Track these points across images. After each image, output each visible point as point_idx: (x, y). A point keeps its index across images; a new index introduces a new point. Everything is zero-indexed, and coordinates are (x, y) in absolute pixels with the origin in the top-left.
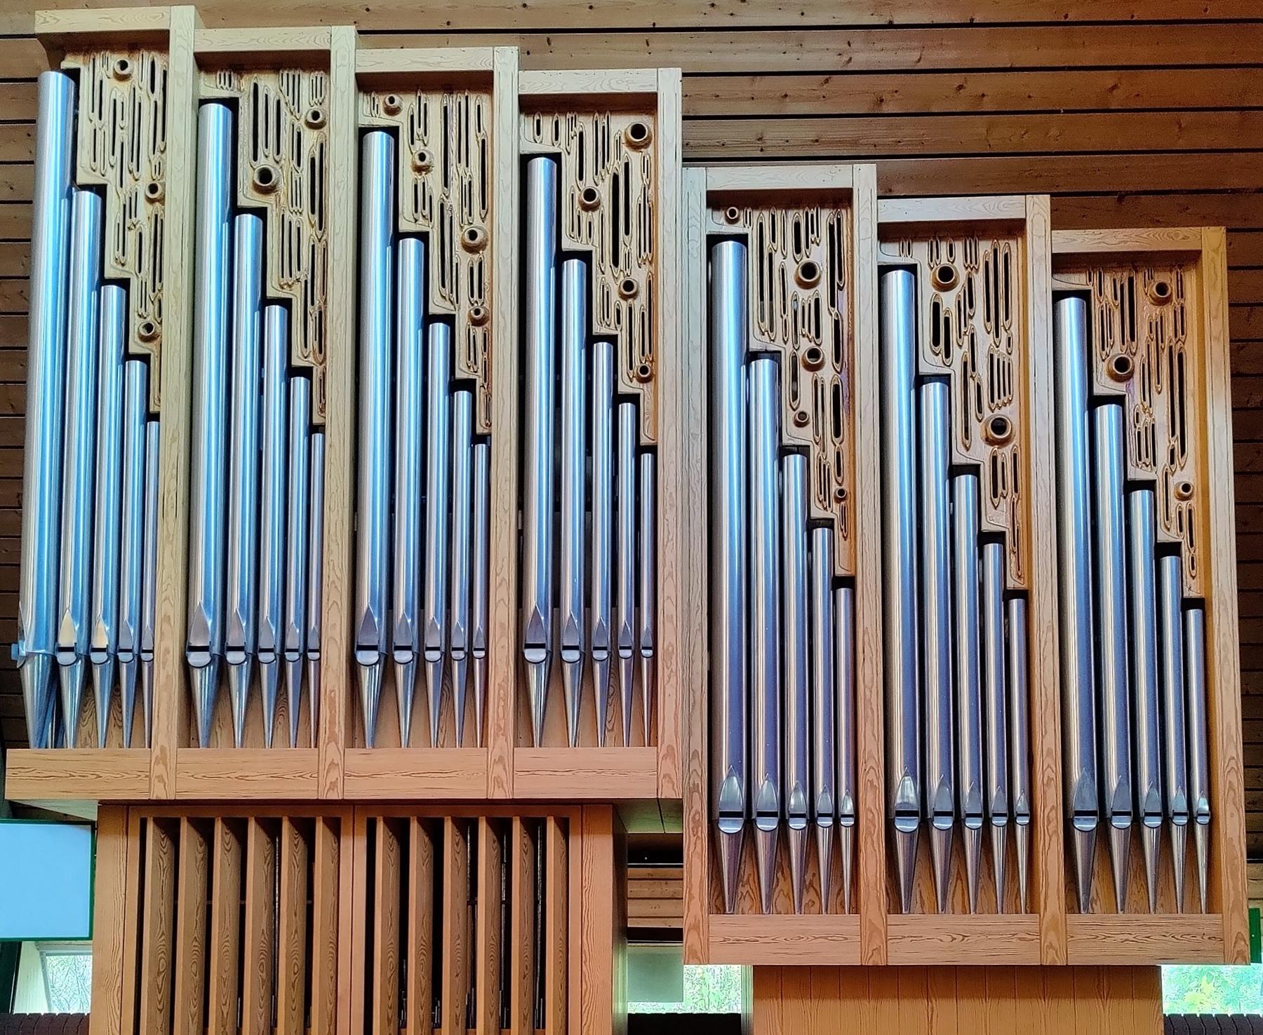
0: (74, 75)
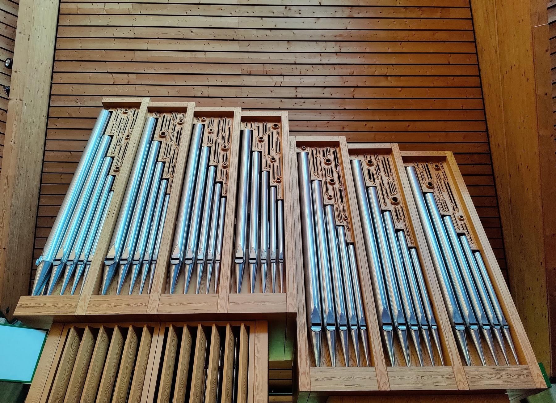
0: (111, 112)
